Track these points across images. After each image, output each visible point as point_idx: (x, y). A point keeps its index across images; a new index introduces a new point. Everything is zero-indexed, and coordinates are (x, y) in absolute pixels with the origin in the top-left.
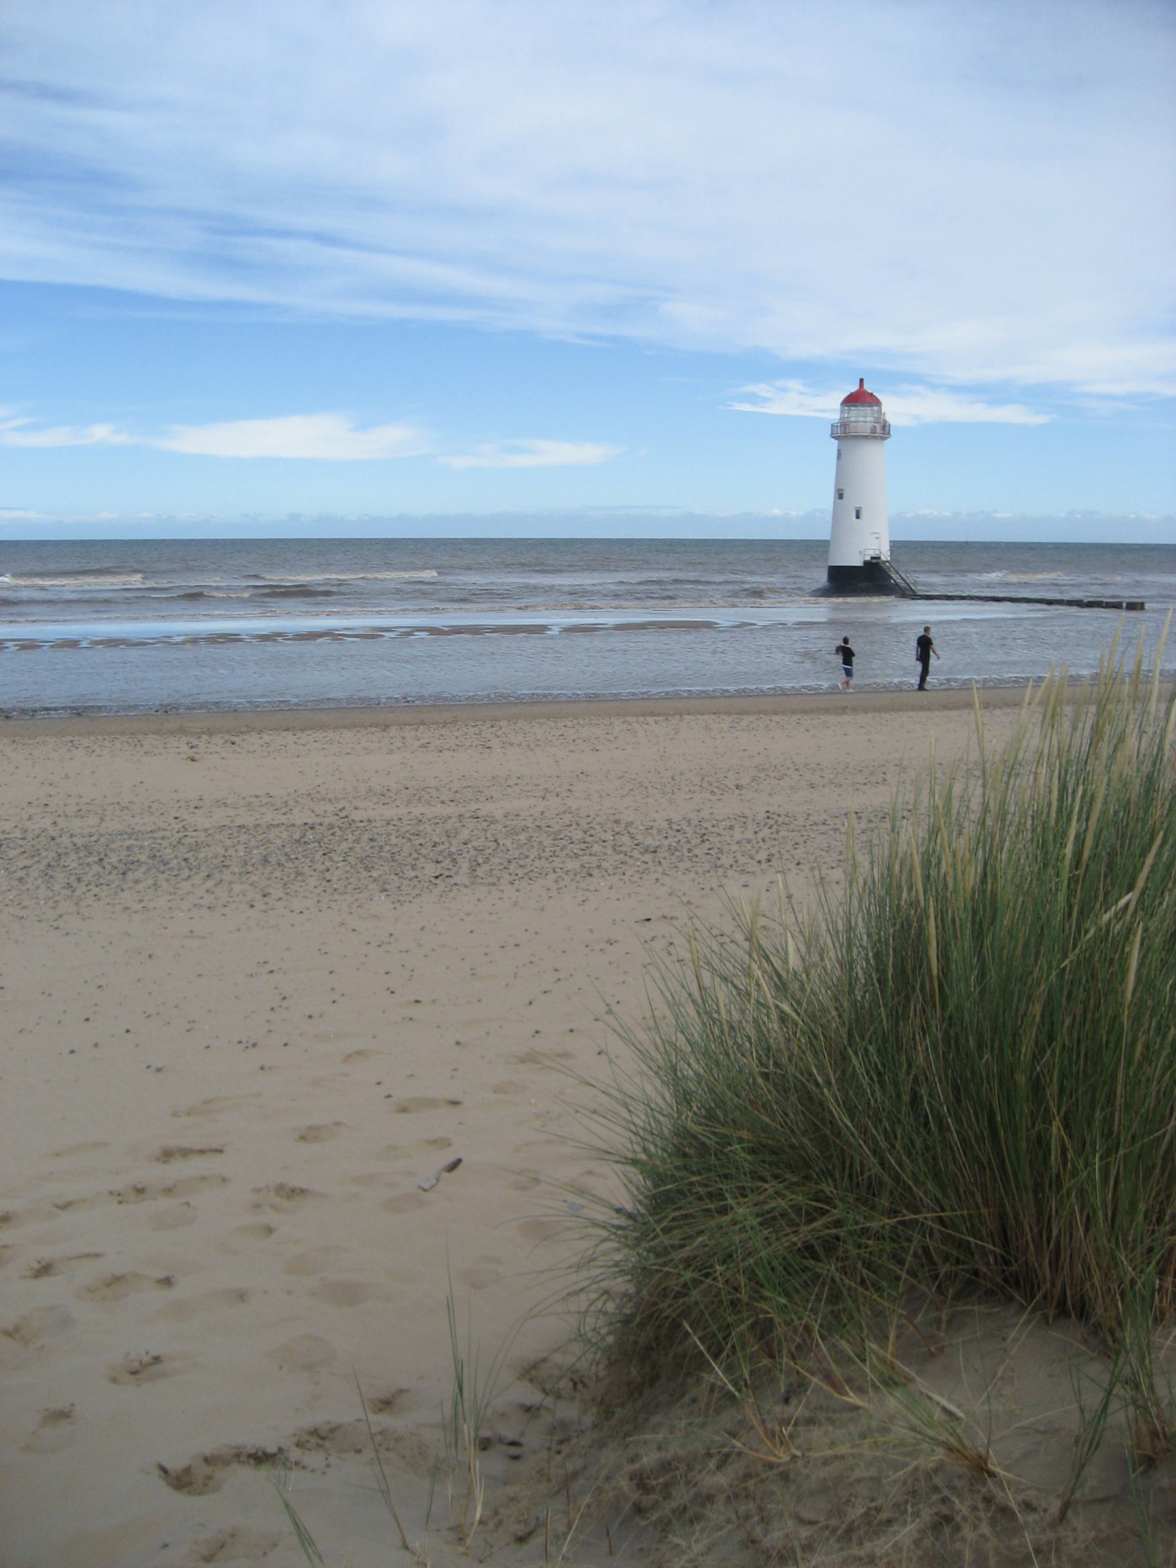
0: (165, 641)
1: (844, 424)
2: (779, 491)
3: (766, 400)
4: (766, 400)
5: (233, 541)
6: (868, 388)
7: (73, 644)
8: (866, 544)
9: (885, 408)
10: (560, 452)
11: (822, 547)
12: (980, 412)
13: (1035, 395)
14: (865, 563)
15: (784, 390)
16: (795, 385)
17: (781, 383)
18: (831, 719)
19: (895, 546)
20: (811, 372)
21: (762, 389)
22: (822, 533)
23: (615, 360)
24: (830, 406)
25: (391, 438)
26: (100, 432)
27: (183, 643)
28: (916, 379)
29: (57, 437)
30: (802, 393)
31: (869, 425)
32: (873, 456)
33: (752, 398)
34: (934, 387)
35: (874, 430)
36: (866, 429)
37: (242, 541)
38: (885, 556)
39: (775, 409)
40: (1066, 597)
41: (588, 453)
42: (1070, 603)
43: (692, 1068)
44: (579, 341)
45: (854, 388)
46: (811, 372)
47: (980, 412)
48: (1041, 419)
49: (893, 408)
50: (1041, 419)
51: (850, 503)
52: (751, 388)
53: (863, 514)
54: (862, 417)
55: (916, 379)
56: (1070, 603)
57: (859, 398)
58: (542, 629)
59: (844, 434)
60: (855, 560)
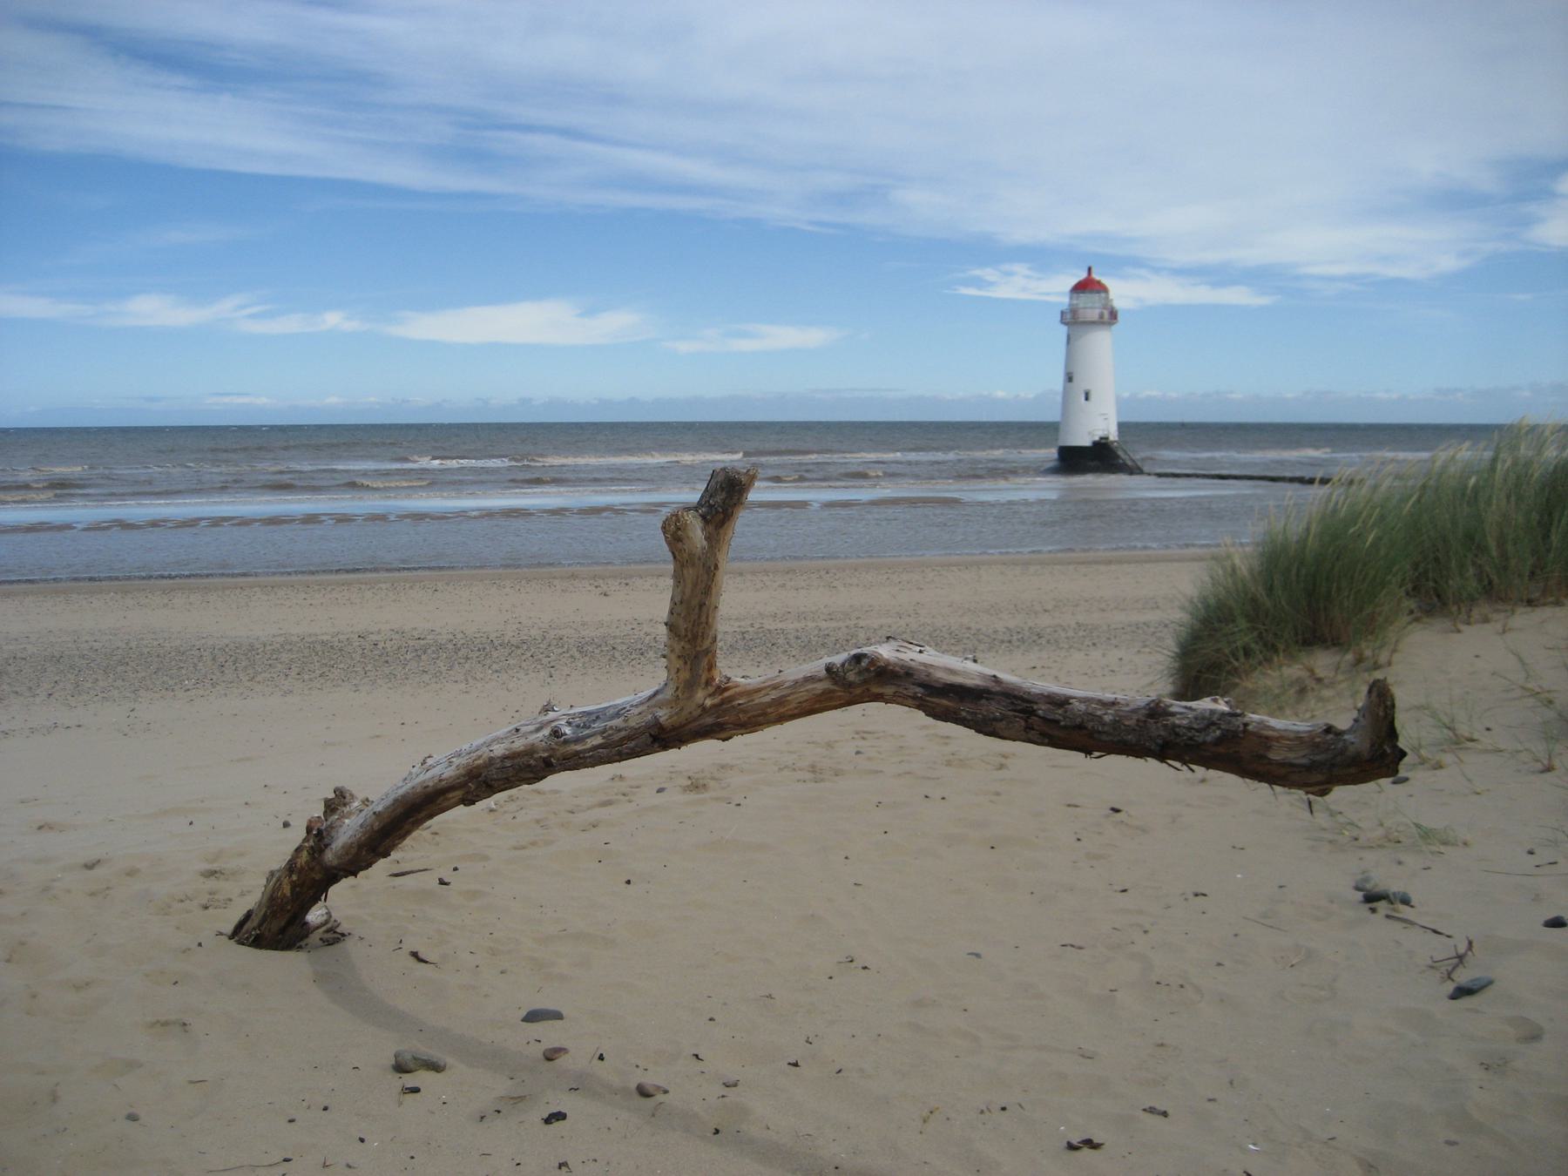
0: (462, 515)
1: (1074, 311)
2: (1010, 374)
3: (991, 284)
4: (991, 284)
5: (450, 426)
6: (1095, 276)
7: (382, 518)
8: (1096, 423)
9: (1112, 295)
10: (786, 337)
11: (1046, 430)
12: (1202, 294)
13: (1256, 276)
14: (1095, 444)
15: (1009, 274)
16: (1021, 269)
17: (1006, 267)
18: (1102, 568)
19: (1123, 427)
20: (1040, 257)
21: (988, 273)
22: (1051, 415)
23: (849, 243)
24: (1057, 289)
25: (617, 323)
26: (333, 319)
27: (482, 517)
28: (1137, 263)
29: (290, 324)
30: (1027, 277)
31: (1097, 312)
32: (1101, 343)
33: (979, 283)
34: (1157, 270)
35: (1101, 316)
36: (1094, 315)
37: (648, 424)
38: (1113, 436)
39: (1005, 291)
40: (1288, 474)
41: (814, 337)
42: (1292, 480)
43: (1212, 601)
44: (810, 228)
45: (1083, 275)
46: (1040, 257)
47: (1202, 294)
48: (1264, 301)
49: (1121, 292)
50: (1264, 301)
51: (1080, 385)
52: (978, 272)
53: (1093, 396)
54: (1090, 306)
55: (1137, 263)
56: (1292, 480)
57: (1087, 286)
58: (803, 504)
59: (1073, 320)
60: (1085, 441)
